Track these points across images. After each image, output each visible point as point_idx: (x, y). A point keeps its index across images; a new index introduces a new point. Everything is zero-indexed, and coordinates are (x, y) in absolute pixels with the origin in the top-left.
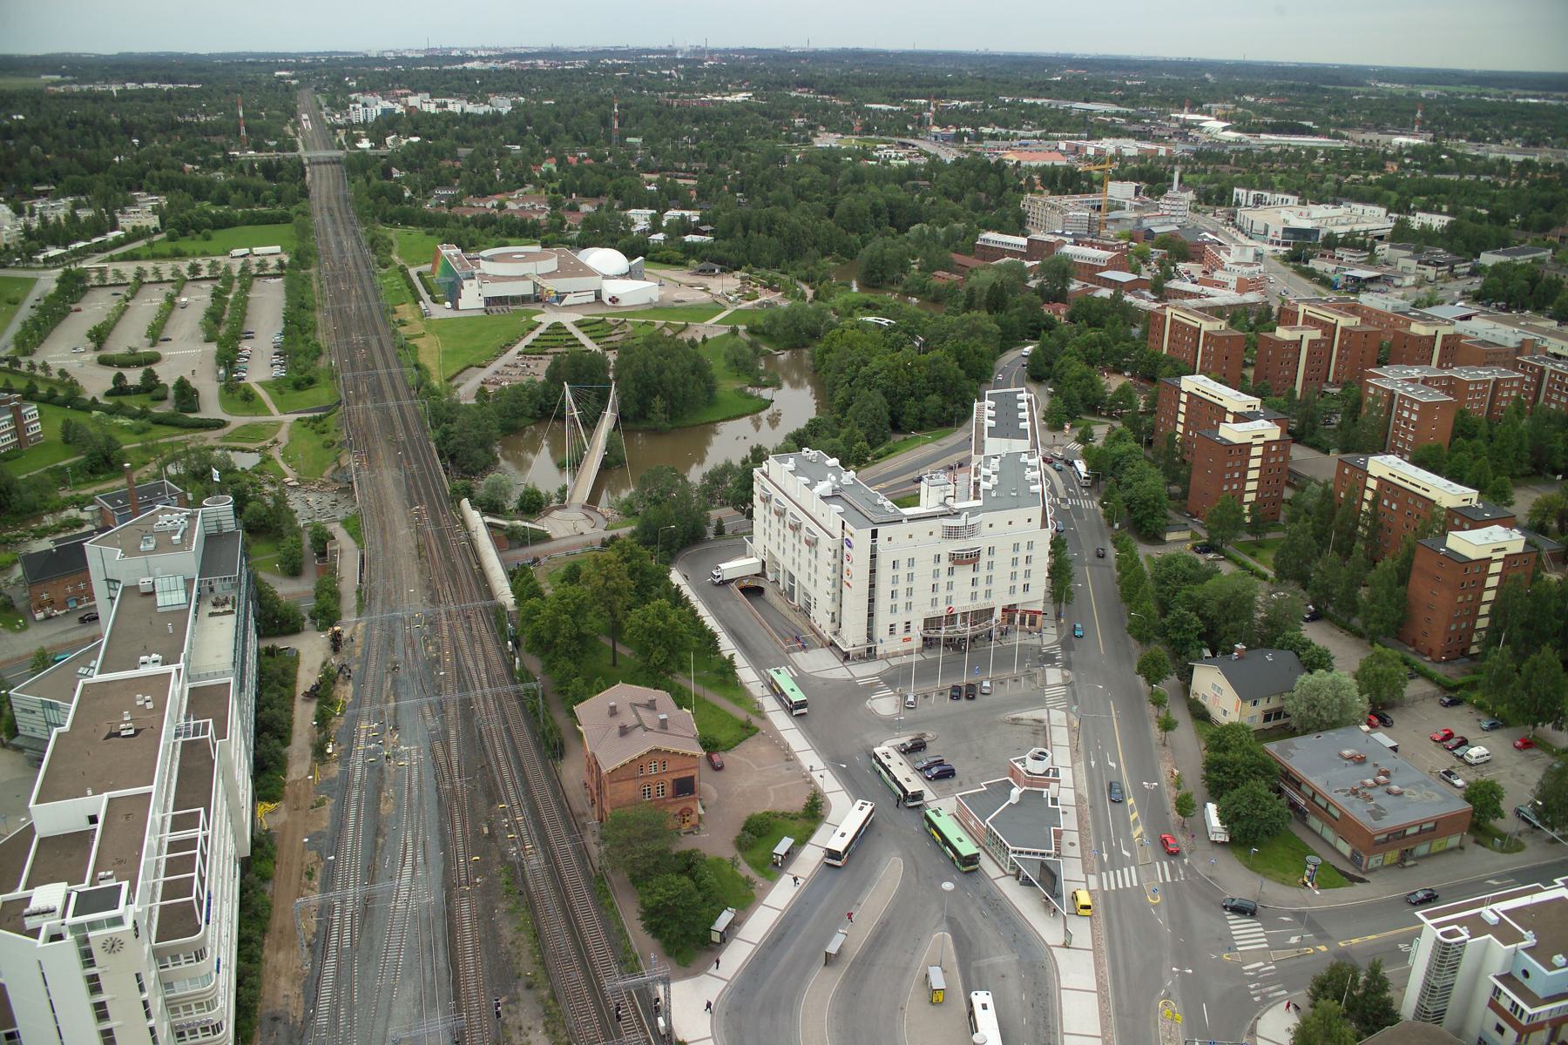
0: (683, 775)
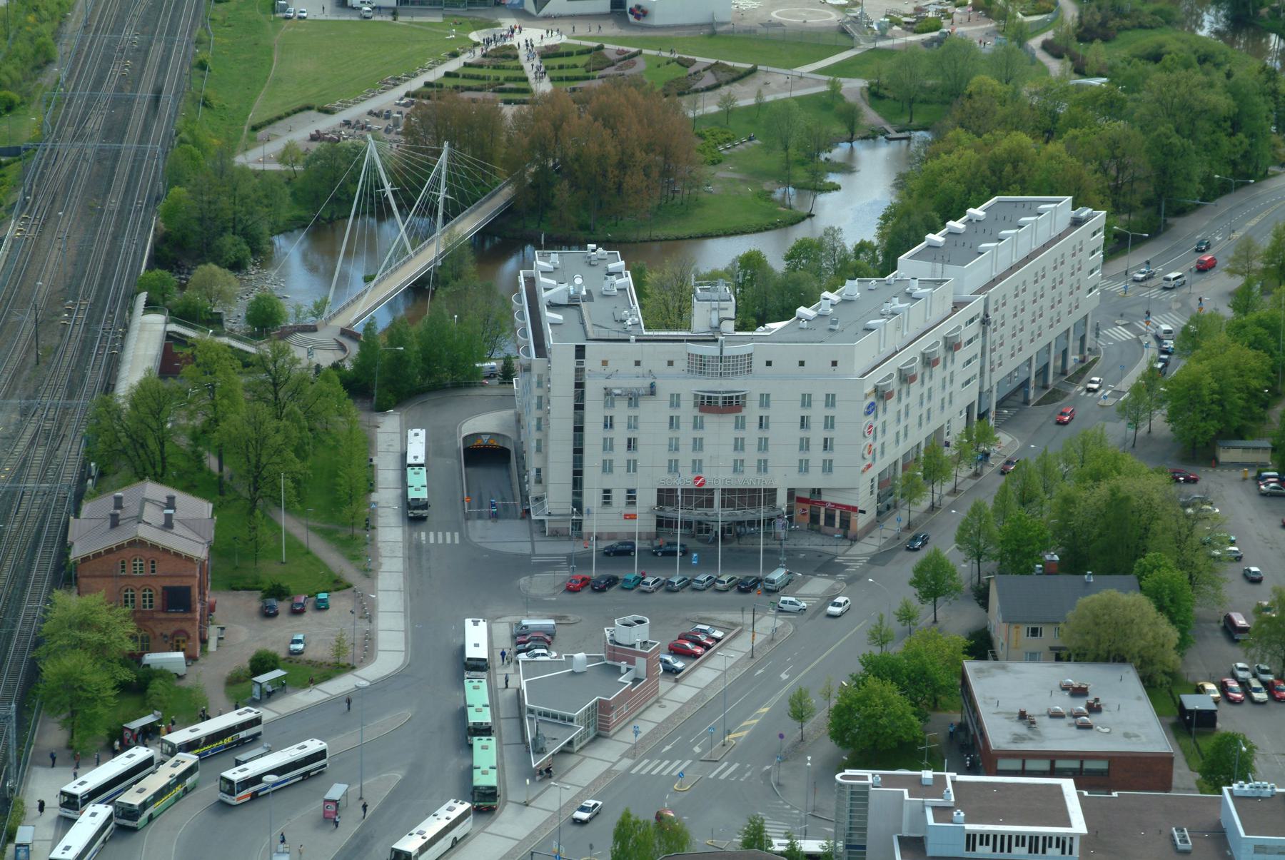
0: (176, 583)
